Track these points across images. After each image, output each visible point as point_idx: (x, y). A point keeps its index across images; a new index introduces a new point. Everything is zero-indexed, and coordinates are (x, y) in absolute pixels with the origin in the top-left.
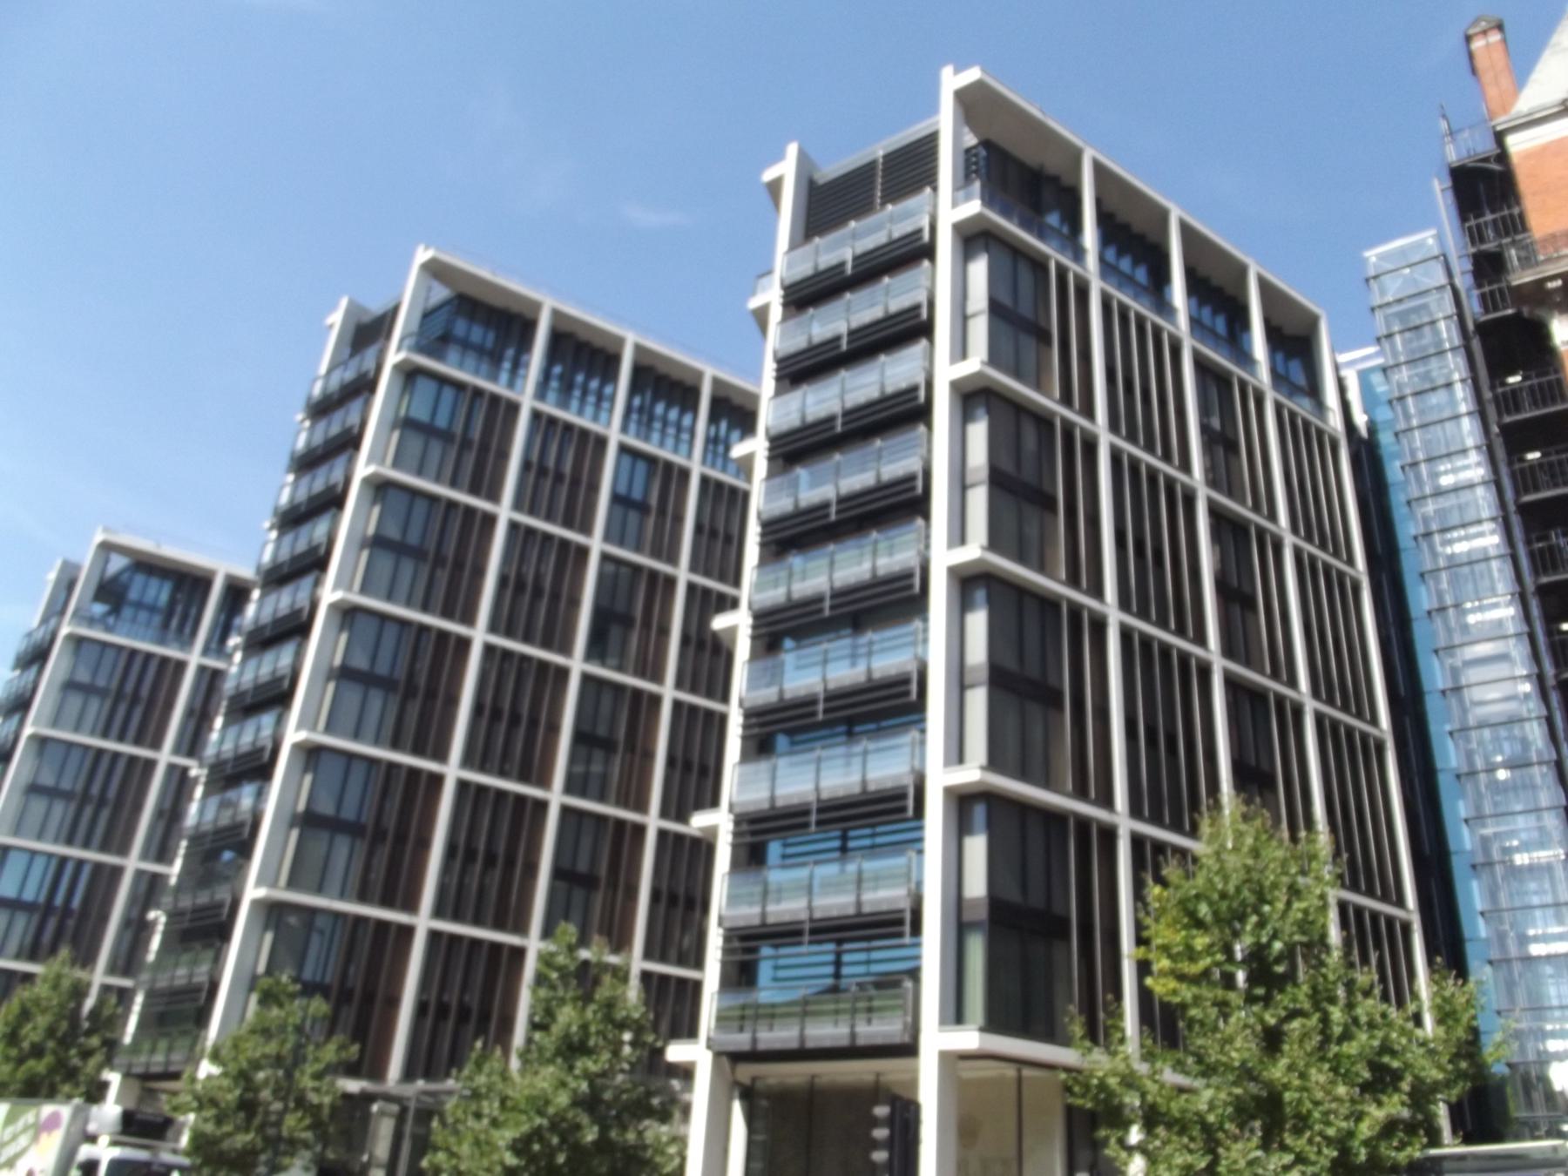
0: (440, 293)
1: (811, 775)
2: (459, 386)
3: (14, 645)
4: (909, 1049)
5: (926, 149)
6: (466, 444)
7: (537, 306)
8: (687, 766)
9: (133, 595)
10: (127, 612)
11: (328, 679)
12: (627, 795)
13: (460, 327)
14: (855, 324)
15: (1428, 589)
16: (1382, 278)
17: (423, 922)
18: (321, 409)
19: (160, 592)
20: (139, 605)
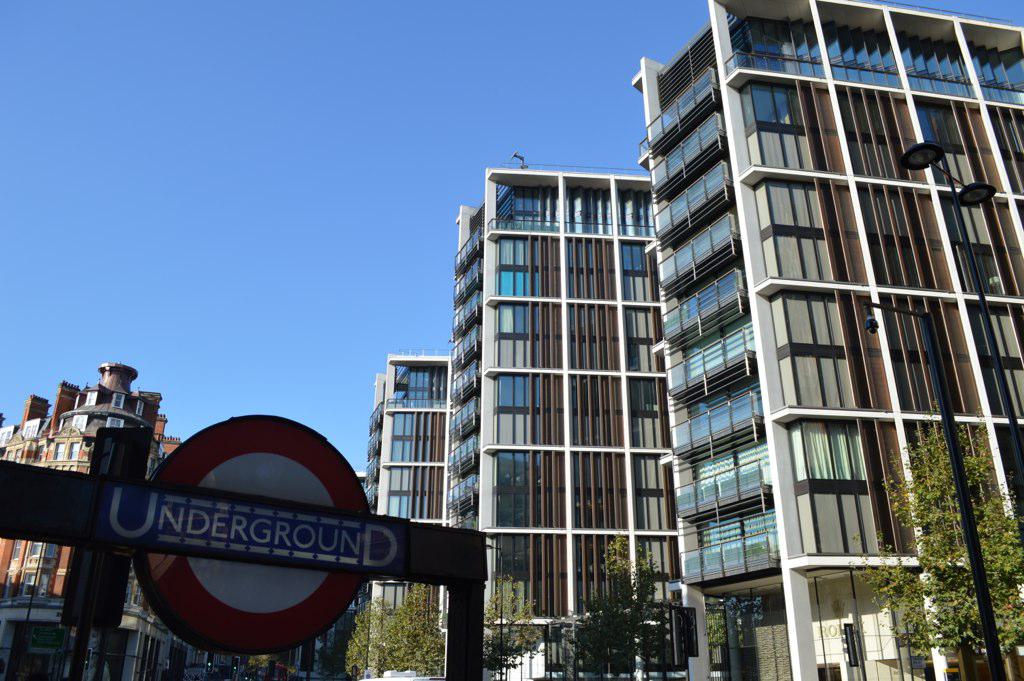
0: (505, 189)
1: (714, 430)
2: (524, 238)
3: (367, 423)
4: (777, 571)
5: (706, 43)
6: (535, 269)
7: (555, 179)
8: (587, 491)
9: (412, 385)
10: (412, 394)
11: (763, 238)
12: (551, 521)
13: (520, 204)
14: (688, 160)
15: (551, 661)
16: (396, 415)
17: (569, 531)
18: (463, 270)
19: (423, 379)
20: (416, 389)
